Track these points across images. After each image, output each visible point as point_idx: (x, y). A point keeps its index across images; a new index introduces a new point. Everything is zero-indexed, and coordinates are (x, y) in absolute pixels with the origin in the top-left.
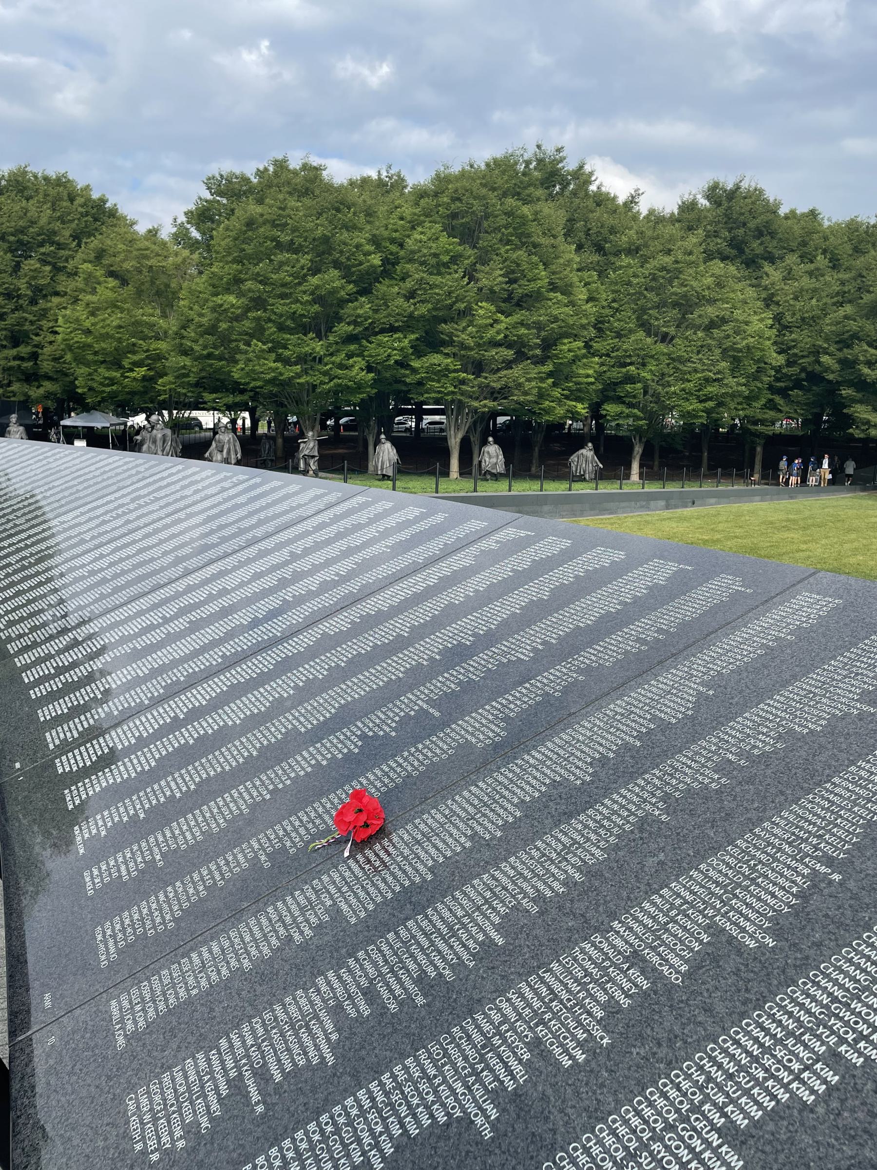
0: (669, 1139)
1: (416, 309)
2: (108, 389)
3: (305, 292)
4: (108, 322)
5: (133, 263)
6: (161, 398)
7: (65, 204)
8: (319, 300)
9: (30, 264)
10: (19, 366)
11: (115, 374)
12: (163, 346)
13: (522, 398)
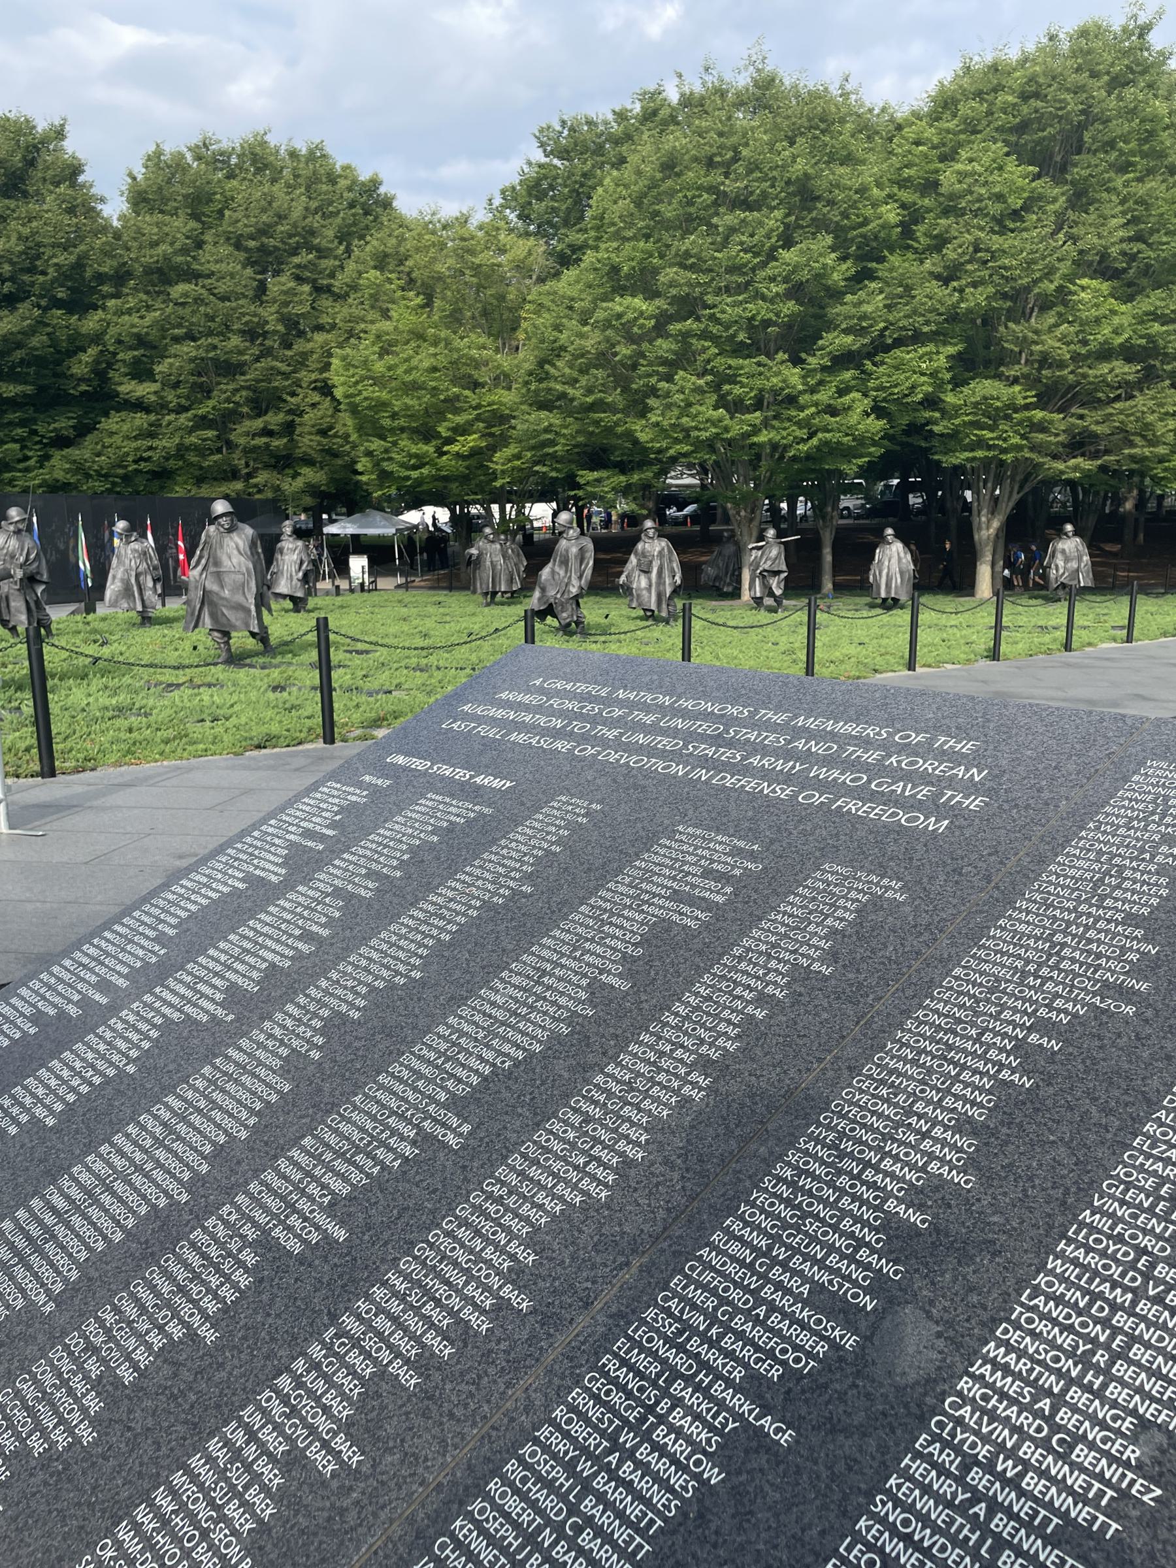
0: (788, 1237)
1: (962, 300)
2: (415, 474)
3: (772, 279)
4: (414, 362)
5: (451, 262)
6: (498, 484)
7: (324, 187)
8: (796, 291)
9: (278, 285)
10: (267, 445)
11: (425, 448)
12: (507, 398)
13: (1147, 451)
